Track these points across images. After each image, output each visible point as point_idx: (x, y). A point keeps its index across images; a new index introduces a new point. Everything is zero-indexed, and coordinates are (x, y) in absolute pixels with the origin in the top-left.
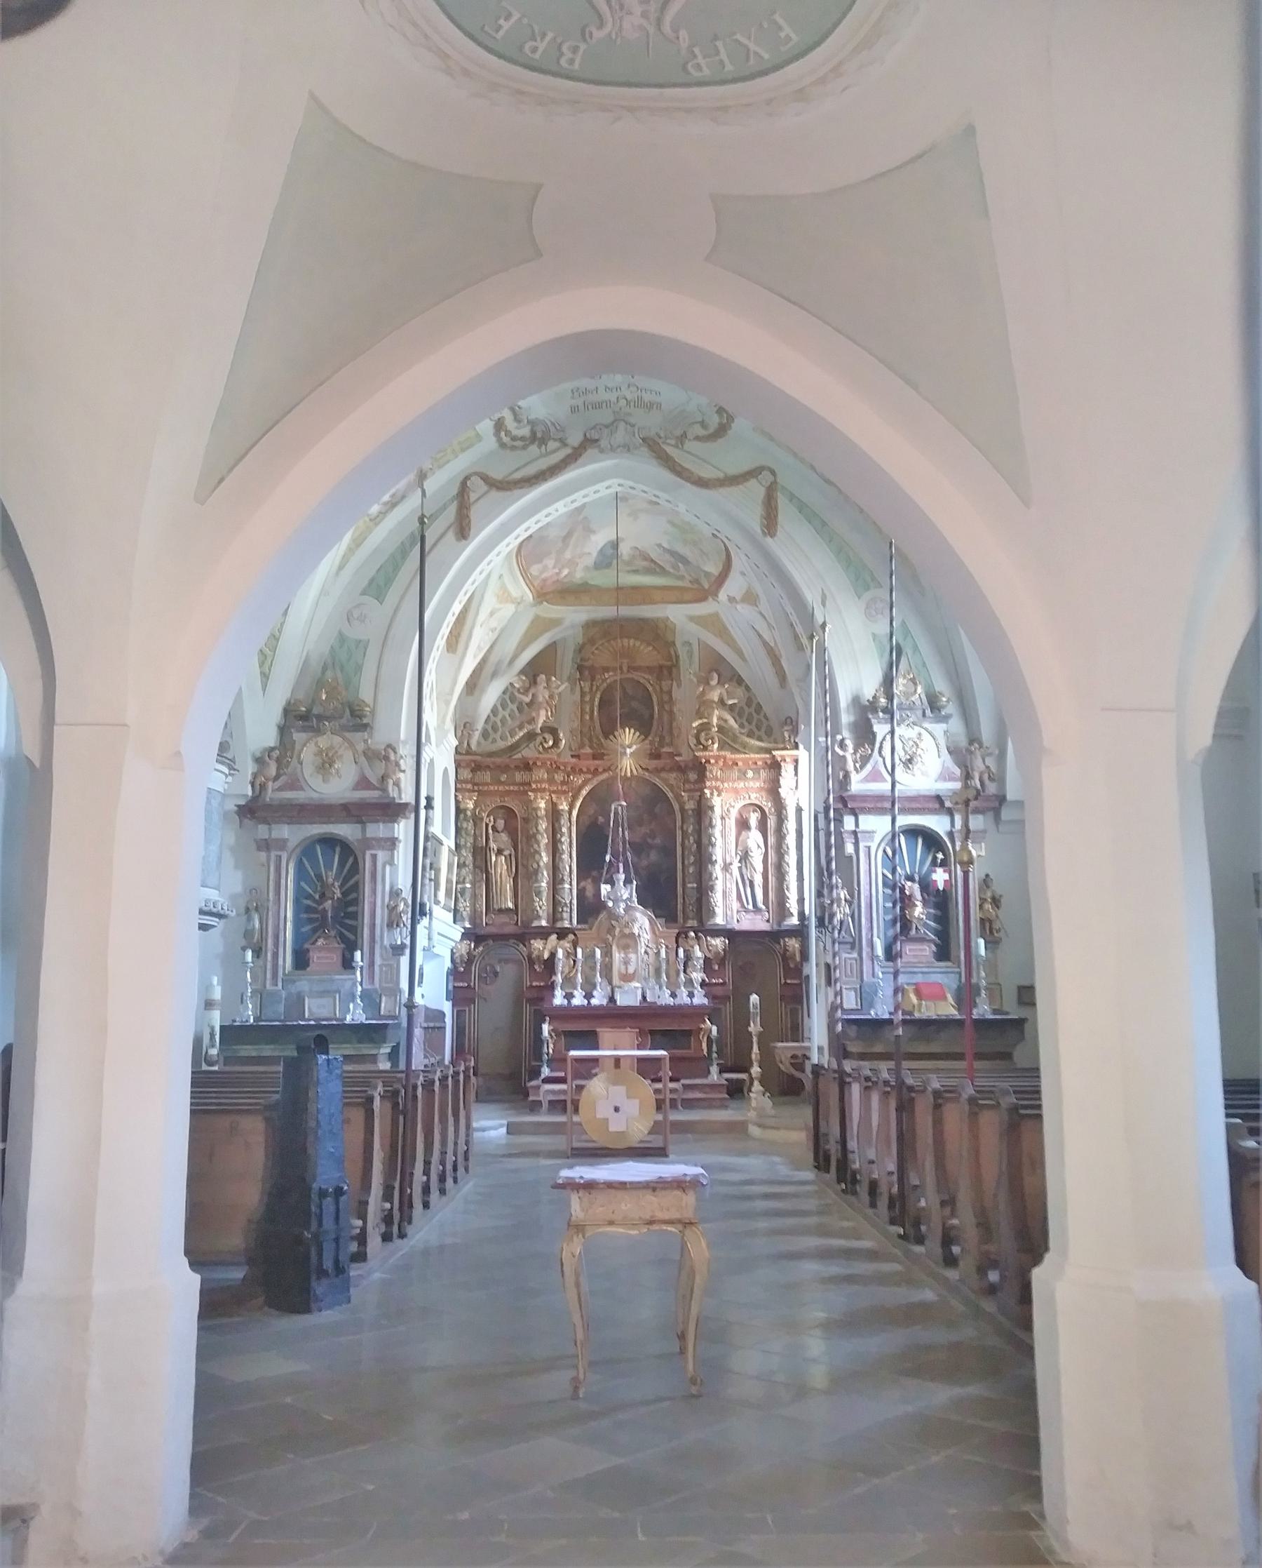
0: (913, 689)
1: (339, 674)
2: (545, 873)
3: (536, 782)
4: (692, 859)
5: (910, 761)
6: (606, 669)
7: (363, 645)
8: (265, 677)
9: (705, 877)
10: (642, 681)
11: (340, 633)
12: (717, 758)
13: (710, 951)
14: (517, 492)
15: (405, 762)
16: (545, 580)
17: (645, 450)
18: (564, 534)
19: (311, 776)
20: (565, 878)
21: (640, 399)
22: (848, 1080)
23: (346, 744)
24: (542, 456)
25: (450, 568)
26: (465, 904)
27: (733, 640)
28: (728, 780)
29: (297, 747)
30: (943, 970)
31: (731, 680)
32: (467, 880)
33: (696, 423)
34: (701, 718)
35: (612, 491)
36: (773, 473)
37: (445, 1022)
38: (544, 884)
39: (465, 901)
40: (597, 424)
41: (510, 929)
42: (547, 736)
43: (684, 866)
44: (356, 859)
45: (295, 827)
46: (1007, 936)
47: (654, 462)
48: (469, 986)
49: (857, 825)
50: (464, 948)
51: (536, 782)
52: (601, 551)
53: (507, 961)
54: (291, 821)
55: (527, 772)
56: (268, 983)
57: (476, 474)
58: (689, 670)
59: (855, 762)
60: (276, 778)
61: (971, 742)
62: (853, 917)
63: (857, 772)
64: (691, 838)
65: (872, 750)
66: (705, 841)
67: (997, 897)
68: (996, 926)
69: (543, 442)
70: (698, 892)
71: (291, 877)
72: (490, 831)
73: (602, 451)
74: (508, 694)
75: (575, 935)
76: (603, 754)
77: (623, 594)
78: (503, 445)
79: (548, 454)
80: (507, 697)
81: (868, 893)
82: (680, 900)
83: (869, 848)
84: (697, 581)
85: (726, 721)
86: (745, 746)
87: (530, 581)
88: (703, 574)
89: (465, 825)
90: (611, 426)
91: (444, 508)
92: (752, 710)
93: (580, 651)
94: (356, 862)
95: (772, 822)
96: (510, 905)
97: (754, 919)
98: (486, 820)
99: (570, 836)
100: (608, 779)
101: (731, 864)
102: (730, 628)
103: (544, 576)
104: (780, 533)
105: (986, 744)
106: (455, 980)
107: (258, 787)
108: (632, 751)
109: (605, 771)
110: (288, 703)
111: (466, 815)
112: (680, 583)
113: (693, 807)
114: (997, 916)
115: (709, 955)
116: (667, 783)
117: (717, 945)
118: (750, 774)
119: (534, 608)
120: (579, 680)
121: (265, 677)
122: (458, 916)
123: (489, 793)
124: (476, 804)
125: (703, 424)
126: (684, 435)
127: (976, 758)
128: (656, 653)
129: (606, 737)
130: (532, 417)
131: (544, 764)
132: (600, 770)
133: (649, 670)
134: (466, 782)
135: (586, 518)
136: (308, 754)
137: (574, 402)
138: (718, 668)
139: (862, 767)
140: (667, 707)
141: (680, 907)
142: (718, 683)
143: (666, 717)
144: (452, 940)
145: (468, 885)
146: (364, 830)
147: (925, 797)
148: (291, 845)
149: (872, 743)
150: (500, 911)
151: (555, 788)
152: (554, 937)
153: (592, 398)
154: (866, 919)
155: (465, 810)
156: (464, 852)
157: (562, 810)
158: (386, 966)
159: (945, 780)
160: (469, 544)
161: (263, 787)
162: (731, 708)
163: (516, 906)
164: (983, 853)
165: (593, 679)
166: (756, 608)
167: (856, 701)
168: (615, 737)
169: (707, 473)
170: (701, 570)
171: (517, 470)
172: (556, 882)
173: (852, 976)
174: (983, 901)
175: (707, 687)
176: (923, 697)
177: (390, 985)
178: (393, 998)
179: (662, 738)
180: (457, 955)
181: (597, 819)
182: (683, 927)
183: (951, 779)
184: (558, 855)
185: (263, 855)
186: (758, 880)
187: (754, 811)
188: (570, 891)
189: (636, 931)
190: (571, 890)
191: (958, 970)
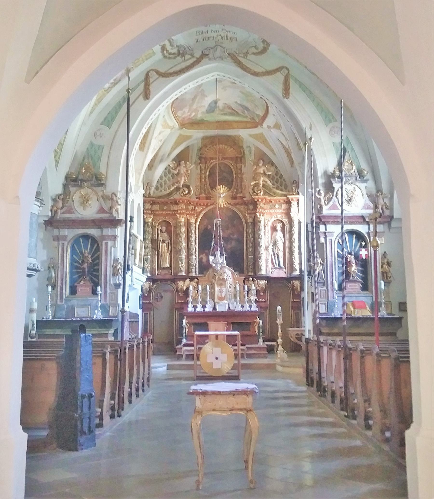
0: (351, 168)
1: (91, 161)
3: (180, 210)
5: (350, 200)
6: (212, 159)
8: (57, 162)
9: (257, 253)
11: (91, 143)
12: (262, 199)
13: (259, 286)
14: (171, 78)
17: (230, 59)
18: (193, 97)
19: (78, 207)
20: (193, 253)
21: (227, 36)
22: (322, 345)
23: (94, 193)
24: (183, 62)
26: (148, 265)
28: (267, 209)
29: (72, 194)
31: (268, 163)
32: (149, 254)
36: (288, 69)
37: (138, 319)
39: (148, 264)
40: (207, 48)
41: (168, 277)
42: (185, 189)
44: (98, 245)
45: (70, 230)
47: (234, 64)
48: (150, 302)
49: (326, 229)
50: (147, 285)
51: (180, 210)
53: (167, 291)
56: (58, 301)
57: (153, 70)
59: (325, 200)
60: (62, 208)
61: (378, 192)
62: (324, 271)
65: (333, 195)
68: (389, 275)
69: (183, 55)
70: (253, 260)
72: (159, 232)
73: (210, 59)
75: (198, 279)
76: (211, 197)
77: (220, 124)
78: (165, 57)
80: (167, 171)
82: (245, 263)
83: (331, 240)
84: (253, 119)
85: (266, 182)
87: (177, 118)
88: (256, 115)
89: (148, 229)
90: (214, 48)
91: (138, 85)
92: (278, 177)
93: (200, 150)
94: (98, 246)
95: (287, 228)
96: (168, 266)
98: (157, 227)
102: (268, 140)
106: (143, 300)
107: (54, 212)
108: (224, 195)
109: (211, 205)
110: (68, 174)
111: (148, 225)
112: (245, 120)
113: (251, 221)
115: (258, 288)
116: (240, 210)
117: (262, 284)
118: (277, 206)
121: (57, 162)
122: (145, 271)
123: (159, 215)
124: (153, 220)
125: (256, 47)
126: (247, 52)
127: (380, 199)
128: (234, 151)
129: (212, 189)
130: (178, 44)
131: (183, 202)
132: (209, 204)
133: (232, 159)
134: (148, 210)
137: (197, 37)
139: (328, 203)
140: (239, 176)
141: (245, 266)
143: (239, 180)
144: (142, 282)
145: (149, 257)
146: (102, 232)
148: (69, 238)
149: (333, 192)
150: (164, 268)
151: (189, 213)
152: (188, 280)
153: (205, 35)
154: (330, 272)
155: (148, 222)
156: (147, 242)
157: (192, 223)
158: (112, 293)
160: (150, 101)
161: (56, 212)
162: (269, 176)
163: (171, 266)
164: (383, 242)
166: (280, 131)
167: (325, 173)
168: (216, 189)
169: (258, 69)
171: (171, 68)
172: (189, 255)
174: (383, 264)
175: (257, 167)
177: (114, 302)
178: (115, 308)
179: (237, 190)
180: (144, 288)
181: (208, 226)
183: (369, 208)
184: (190, 243)
185: (56, 243)
186: (281, 254)
189: (225, 277)
190: (196, 259)
191: (372, 295)
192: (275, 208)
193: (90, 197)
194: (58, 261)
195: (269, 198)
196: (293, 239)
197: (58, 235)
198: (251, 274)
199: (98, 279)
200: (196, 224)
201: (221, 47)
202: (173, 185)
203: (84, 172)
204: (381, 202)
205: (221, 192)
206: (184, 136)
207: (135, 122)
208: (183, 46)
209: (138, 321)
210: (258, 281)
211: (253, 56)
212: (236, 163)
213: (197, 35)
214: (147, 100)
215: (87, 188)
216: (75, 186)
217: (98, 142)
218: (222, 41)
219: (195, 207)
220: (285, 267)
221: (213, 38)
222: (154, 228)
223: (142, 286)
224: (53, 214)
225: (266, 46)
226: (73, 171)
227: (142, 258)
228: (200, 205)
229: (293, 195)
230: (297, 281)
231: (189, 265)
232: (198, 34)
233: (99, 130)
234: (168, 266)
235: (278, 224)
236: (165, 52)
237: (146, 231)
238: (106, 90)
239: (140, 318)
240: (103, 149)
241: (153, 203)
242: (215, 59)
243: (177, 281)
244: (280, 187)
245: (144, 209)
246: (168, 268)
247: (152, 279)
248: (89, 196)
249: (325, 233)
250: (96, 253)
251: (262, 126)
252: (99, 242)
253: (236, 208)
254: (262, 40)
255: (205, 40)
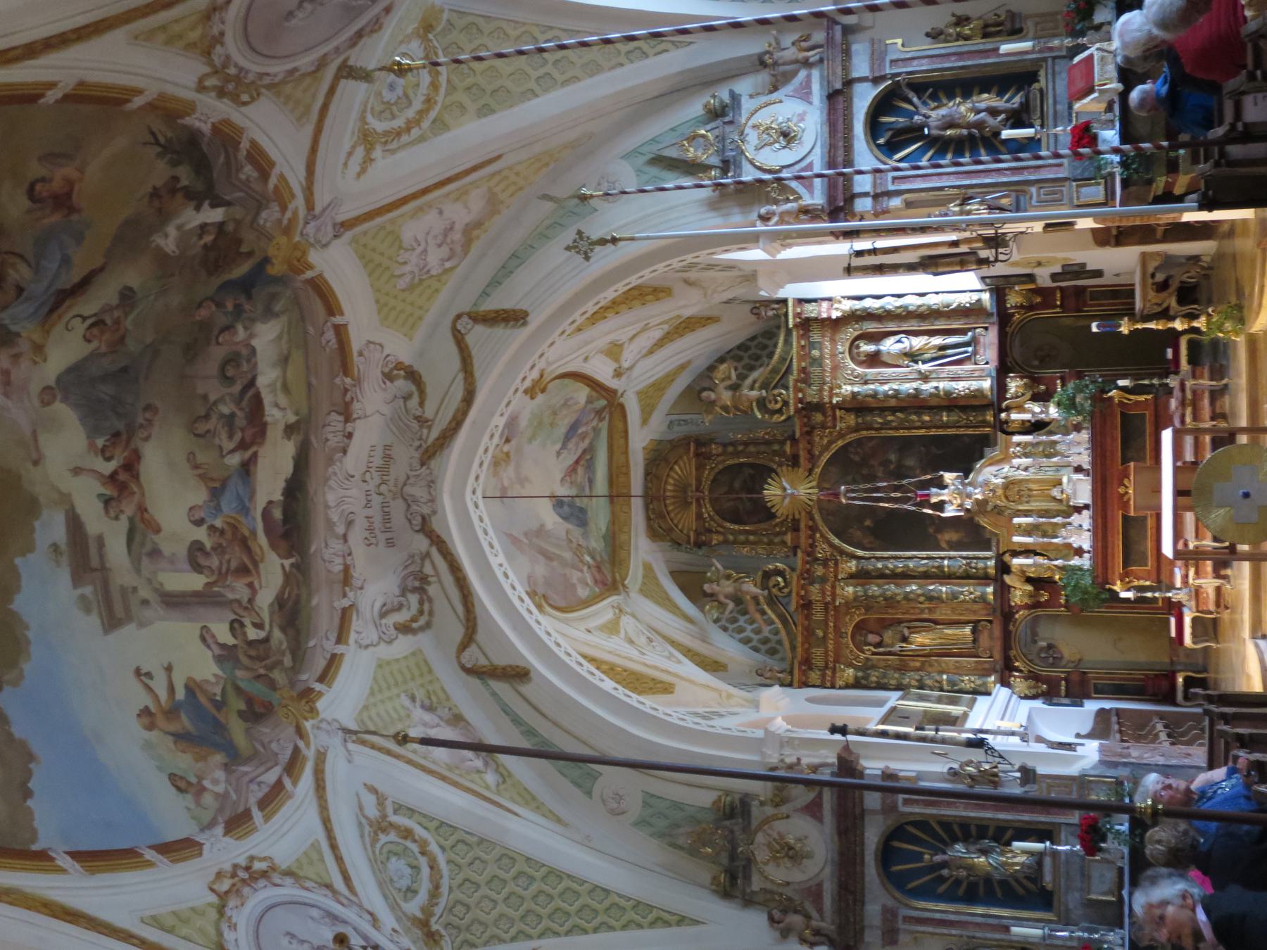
0: (701, 140)
1: (682, 830)
2: (932, 587)
3: (824, 597)
4: (914, 417)
5: (785, 134)
6: (699, 516)
7: (649, 800)
8: (682, 920)
9: (934, 402)
10: (711, 477)
11: (636, 824)
12: (798, 390)
13: (1023, 395)
14: (478, 610)
15: (787, 756)
16: (596, 582)
17: (433, 463)
18: (541, 558)
19: (804, 872)
20: (936, 564)
21: (379, 469)
22: (1240, 126)
23: (766, 827)
24: (440, 582)
25: (562, 692)
27: (667, 375)
28: (823, 378)
29: (769, 886)
30: (1050, 77)
31: (711, 378)
32: (938, 678)
33: (405, 405)
34: (752, 410)
35: (481, 502)
36: (459, 317)
37: (1111, 709)
38: (944, 589)
40: (407, 518)
41: (997, 630)
42: (771, 583)
43: (920, 427)
44: (907, 823)
45: (868, 897)
46: (1003, 5)
47: (446, 452)
48: (1066, 679)
49: (866, 194)
50: (1019, 684)
51: (824, 597)
52: (565, 518)
53: (1034, 634)
54: (860, 901)
55: (814, 606)
57: (458, 657)
58: (706, 423)
59: (788, 200)
60: (808, 917)
61: (763, 64)
63: (800, 198)
64: (890, 418)
66: (893, 403)
67: (954, 19)
68: (991, 18)
69: (424, 579)
70: (952, 411)
71: (931, 905)
72: (881, 650)
73: (434, 512)
74: (727, 625)
75: (1004, 553)
76: (794, 519)
77: (618, 495)
78: (428, 625)
79: (437, 574)
80: (731, 627)
81: (952, 177)
82: (962, 431)
84: (599, 413)
85: (755, 382)
86: (783, 359)
88: (590, 406)
89: (874, 679)
90: (408, 502)
91: (494, 694)
92: (746, 355)
93: (679, 544)
94: (915, 824)
95: (871, 327)
97: (984, 344)
98: (868, 654)
99: (888, 558)
100: (821, 514)
101: (920, 372)
102: (652, 380)
103: (590, 581)
104: (523, 306)
105: (766, 47)
106: (1058, 695)
107: (817, 938)
109: (812, 518)
110: (715, 892)
111: (863, 678)
112: (604, 434)
113: (853, 417)
114: (980, 18)
115: (1028, 395)
116: (827, 448)
117: (1017, 386)
118: (815, 353)
119: (631, 594)
120: (711, 546)
121: (682, 920)
122: (983, 689)
124: (850, 665)
125: (406, 398)
126: (418, 418)
127: (782, 57)
129: (773, 516)
130: (397, 592)
131: (803, 587)
132: (811, 523)
133: (700, 468)
134: (823, 676)
135: (526, 534)
136: (779, 873)
137: (382, 544)
138: (697, 393)
139: (794, 192)
140: (740, 448)
141: (970, 432)
142: (712, 390)
143: (752, 449)
144: (1009, 701)
145: (945, 677)
146: (874, 812)
147: (829, 114)
148: (890, 903)
150: (975, 641)
151: (832, 575)
152: (1007, 579)
153: (378, 520)
154: (986, 177)
155: (856, 678)
156: (906, 681)
157: (857, 567)
159: (810, 93)
160: (533, 667)
161: (817, 932)
162: (742, 377)
163: (967, 622)
164: (899, 41)
165: (710, 531)
166: (626, 345)
167: (713, 205)
169: (458, 393)
170: (585, 407)
171: (455, 612)
173: (1062, 191)
174: (960, 37)
175: (718, 404)
176: (709, 127)
177: (1075, 788)
178: (1093, 786)
179: (775, 453)
180: (1027, 692)
181: (868, 527)
182: (994, 427)
183: (808, 83)
185: (903, 938)
186: (938, 341)
187: (858, 347)
188: (952, 559)
189: (999, 481)
190: (950, 558)
191: (1050, 61)
192: (822, 357)
193: (777, 837)
194: (954, 936)
195: (795, 372)
196: (899, 311)
197: (879, 932)
198: (990, 418)
199: (1008, 828)
200: (859, 558)
201: (405, 484)
202: (763, 613)
203: (710, 850)
204: (791, 53)
205: (779, 492)
206: (644, 583)
207: (587, 709)
208: (405, 579)
209: (1117, 710)
210: (1008, 396)
211: (427, 403)
212: (708, 457)
213: (377, 545)
214: (532, 674)
215: (752, 844)
216: (747, 878)
217: (634, 807)
218: (391, 483)
219: (817, 559)
220: (970, 329)
221: (384, 505)
222: (870, 663)
223: (1022, 698)
224: (823, 939)
225: (402, 373)
226: (706, 877)
227: (947, 696)
228: (813, 546)
229: (786, 314)
230: (1008, 297)
231: (967, 576)
232: (373, 540)
233: (604, 801)
234: (967, 630)
235: (862, 349)
236: (415, 625)
237: (876, 682)
238: (501, 780)
239: (1108, 705)
240: (653, 796)
241: (807, 662)
242: (432, 501)
243: (1010, 606)
244: (770, 349)
245: (823, 686)
246: (974, 631)
247: (1005, 675)
248: (774, 839)
249: (876, 197)
250: (933, 829)
251: (619, 394)
252: (903, 821)
253: (821, 454)
254: (388, 383)
255: (388, 525)
